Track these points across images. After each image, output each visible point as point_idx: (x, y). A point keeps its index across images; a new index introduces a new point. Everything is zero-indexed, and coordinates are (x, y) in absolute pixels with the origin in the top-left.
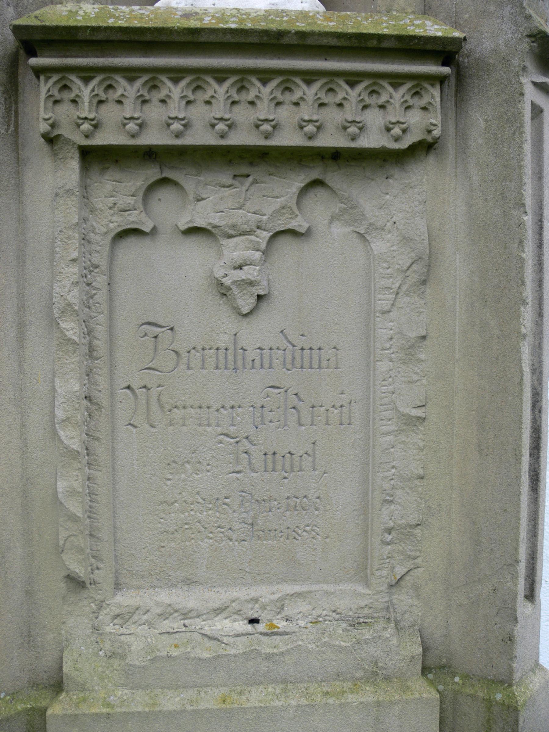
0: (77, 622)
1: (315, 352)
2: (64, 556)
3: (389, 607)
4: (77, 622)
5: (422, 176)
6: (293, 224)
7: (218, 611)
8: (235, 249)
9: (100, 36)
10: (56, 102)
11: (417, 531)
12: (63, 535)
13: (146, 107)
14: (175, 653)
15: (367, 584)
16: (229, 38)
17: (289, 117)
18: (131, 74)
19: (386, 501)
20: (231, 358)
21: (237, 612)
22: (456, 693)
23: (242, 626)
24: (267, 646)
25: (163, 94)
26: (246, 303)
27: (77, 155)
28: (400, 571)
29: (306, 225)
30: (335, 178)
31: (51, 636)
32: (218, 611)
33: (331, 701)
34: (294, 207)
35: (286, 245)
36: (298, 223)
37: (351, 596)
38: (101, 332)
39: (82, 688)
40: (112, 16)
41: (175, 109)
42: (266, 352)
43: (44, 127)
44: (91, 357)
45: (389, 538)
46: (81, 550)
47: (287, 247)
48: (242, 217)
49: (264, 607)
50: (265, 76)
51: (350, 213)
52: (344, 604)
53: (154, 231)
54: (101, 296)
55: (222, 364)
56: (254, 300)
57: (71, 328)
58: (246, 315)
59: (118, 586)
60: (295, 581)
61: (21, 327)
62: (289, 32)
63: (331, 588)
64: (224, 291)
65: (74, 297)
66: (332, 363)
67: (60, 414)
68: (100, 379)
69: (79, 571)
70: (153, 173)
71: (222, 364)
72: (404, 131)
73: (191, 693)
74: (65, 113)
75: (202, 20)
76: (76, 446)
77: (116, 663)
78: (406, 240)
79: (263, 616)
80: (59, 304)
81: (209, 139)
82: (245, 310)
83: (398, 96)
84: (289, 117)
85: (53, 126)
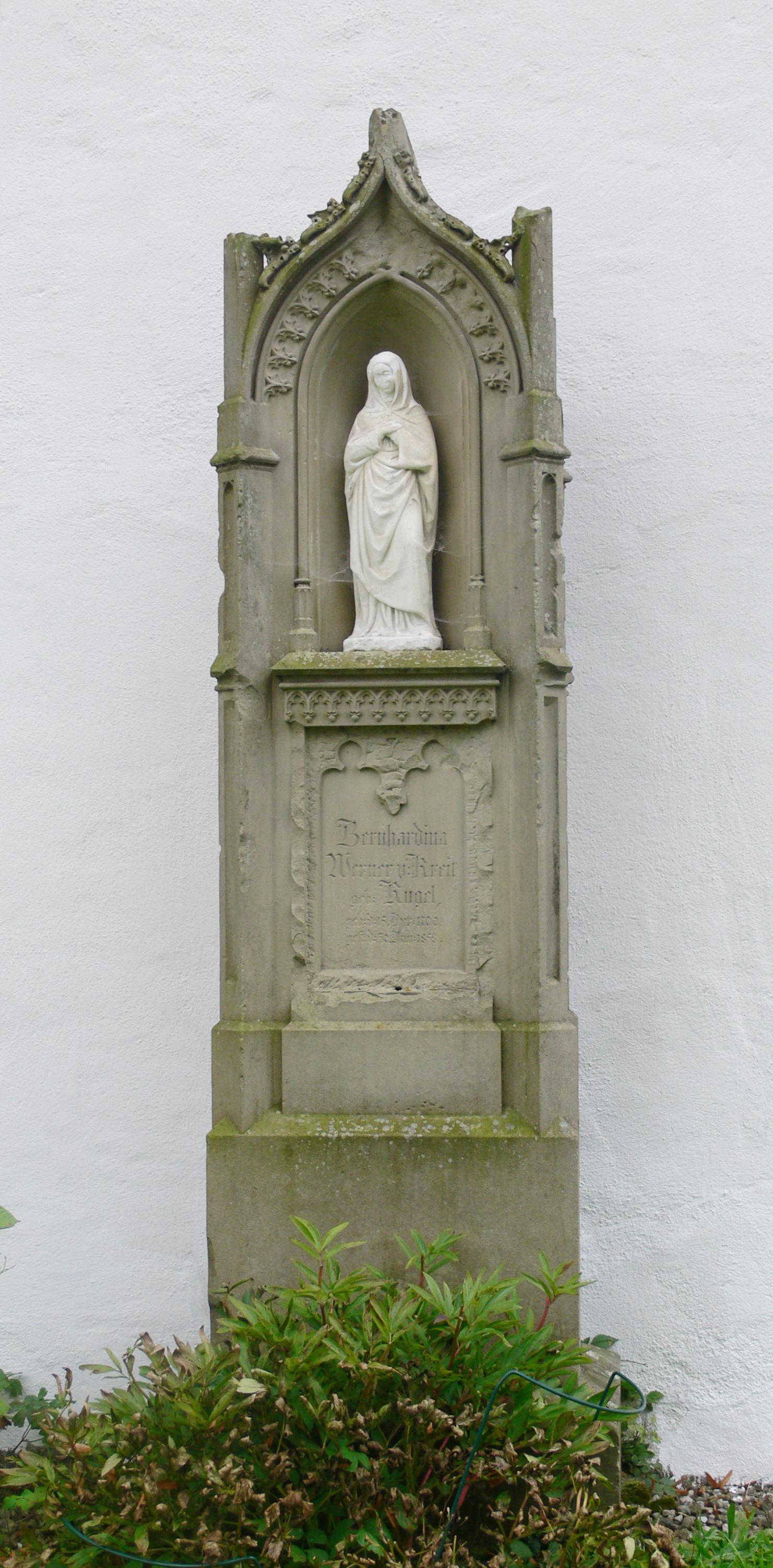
0: (300, 985)
1: (433, 835)
2: (294, 946)
3: (476, 983)
4: (300, 985)
5: (490, 737)
6: (419, 765)
7: (378, 982)
8: (388, 779)
9: (315, 673)
10: (293, 704)
11: (490, 937)
12: (294, 934)
13: (339, 706)
14: (352, 1001)
15: (464, 968)
16: (380, 672)
17: (394, 710)
18: (331, 690)
19: (473, 920)
20: (386, 839)
21: (389, 983)
22: (513, 1032)
23: (393, 990)
24: (403, 999)
25: (348, 699)
26: (394, 808)
27: (303, 731)
28: (482, 961)
29: (427, 765)
30: (442, 739)
31: (285, 992)
32: (378, 982)
33: (437, 1029)
34: (420, 756)
35: (416, 777)
36: (422, 764)
37: (454, 976)
38: (316, 824)
39: (302, 1020)
40: (321, 661)
41: (354, 708)
42: (406, 835)
43: (287, 718)
44: (311, 838)
45: (475, 941)
46: (303, 942)
47: (417, 778)
48: (392, 762)
49: (404, 980)
50: (400, 689)
51: (451, 758)
52: (450, 980)
53: (345, 769)
54: (316, 805)
55: (382, 842)
56: (398, 807)
57: (300, 822)
58: (395, 815)
59: (322, 967)
60: (423, 967)
61: (274, 822)
62: (409, 669)
63: (443, 971)
64: (382, 802)
65: (302, 805)
66: (443, 841)
67: (294, 867)
68: (315, 849)
69: (302, 954)
70: (343, 739)
71: (382, 842)
72: (476, 715)
73: (361, 1023)
74: (297, 709)
75: (366, 662)
76: (302, 884)
77: (320, 1007)
78: (481, 773)
79: (404, 985)
80: (294, 809)
81: (442, 722)
82: (394, 812)
83: (471, 696)
84: (414, 711)
85: (291, 717)
